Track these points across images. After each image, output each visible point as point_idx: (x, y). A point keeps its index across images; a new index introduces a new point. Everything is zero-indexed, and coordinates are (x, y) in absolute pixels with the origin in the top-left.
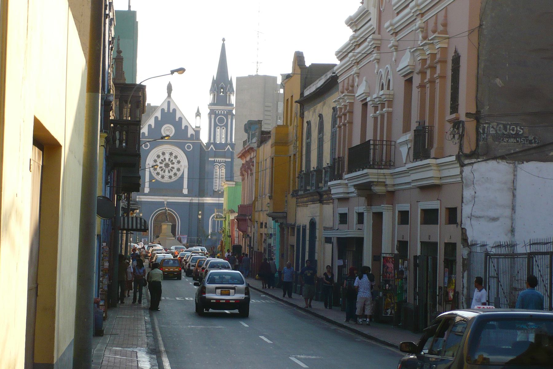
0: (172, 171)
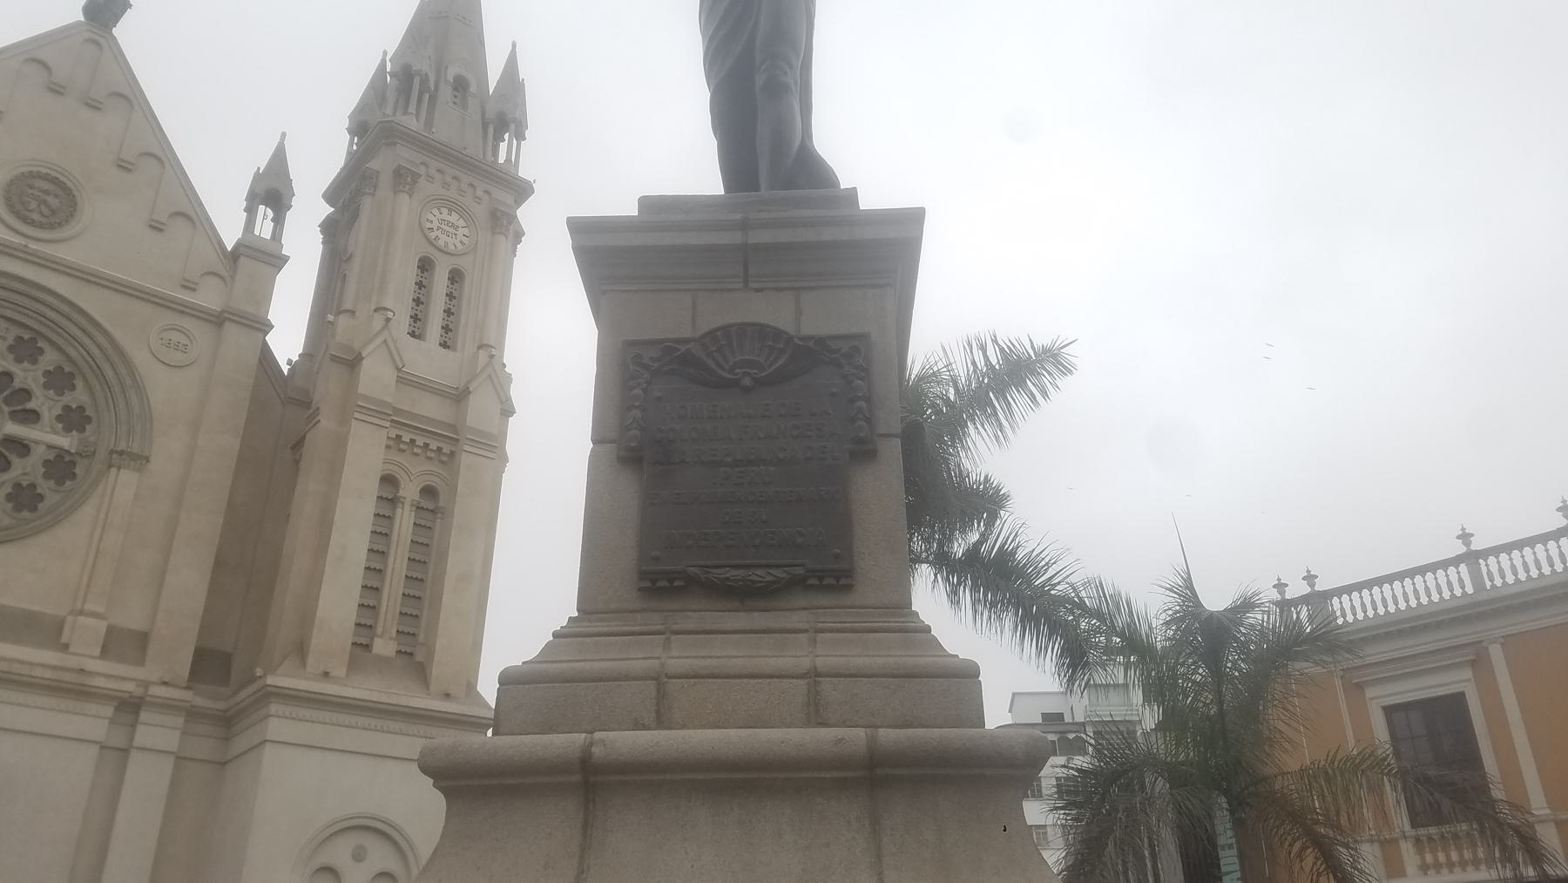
0: (26, 394)
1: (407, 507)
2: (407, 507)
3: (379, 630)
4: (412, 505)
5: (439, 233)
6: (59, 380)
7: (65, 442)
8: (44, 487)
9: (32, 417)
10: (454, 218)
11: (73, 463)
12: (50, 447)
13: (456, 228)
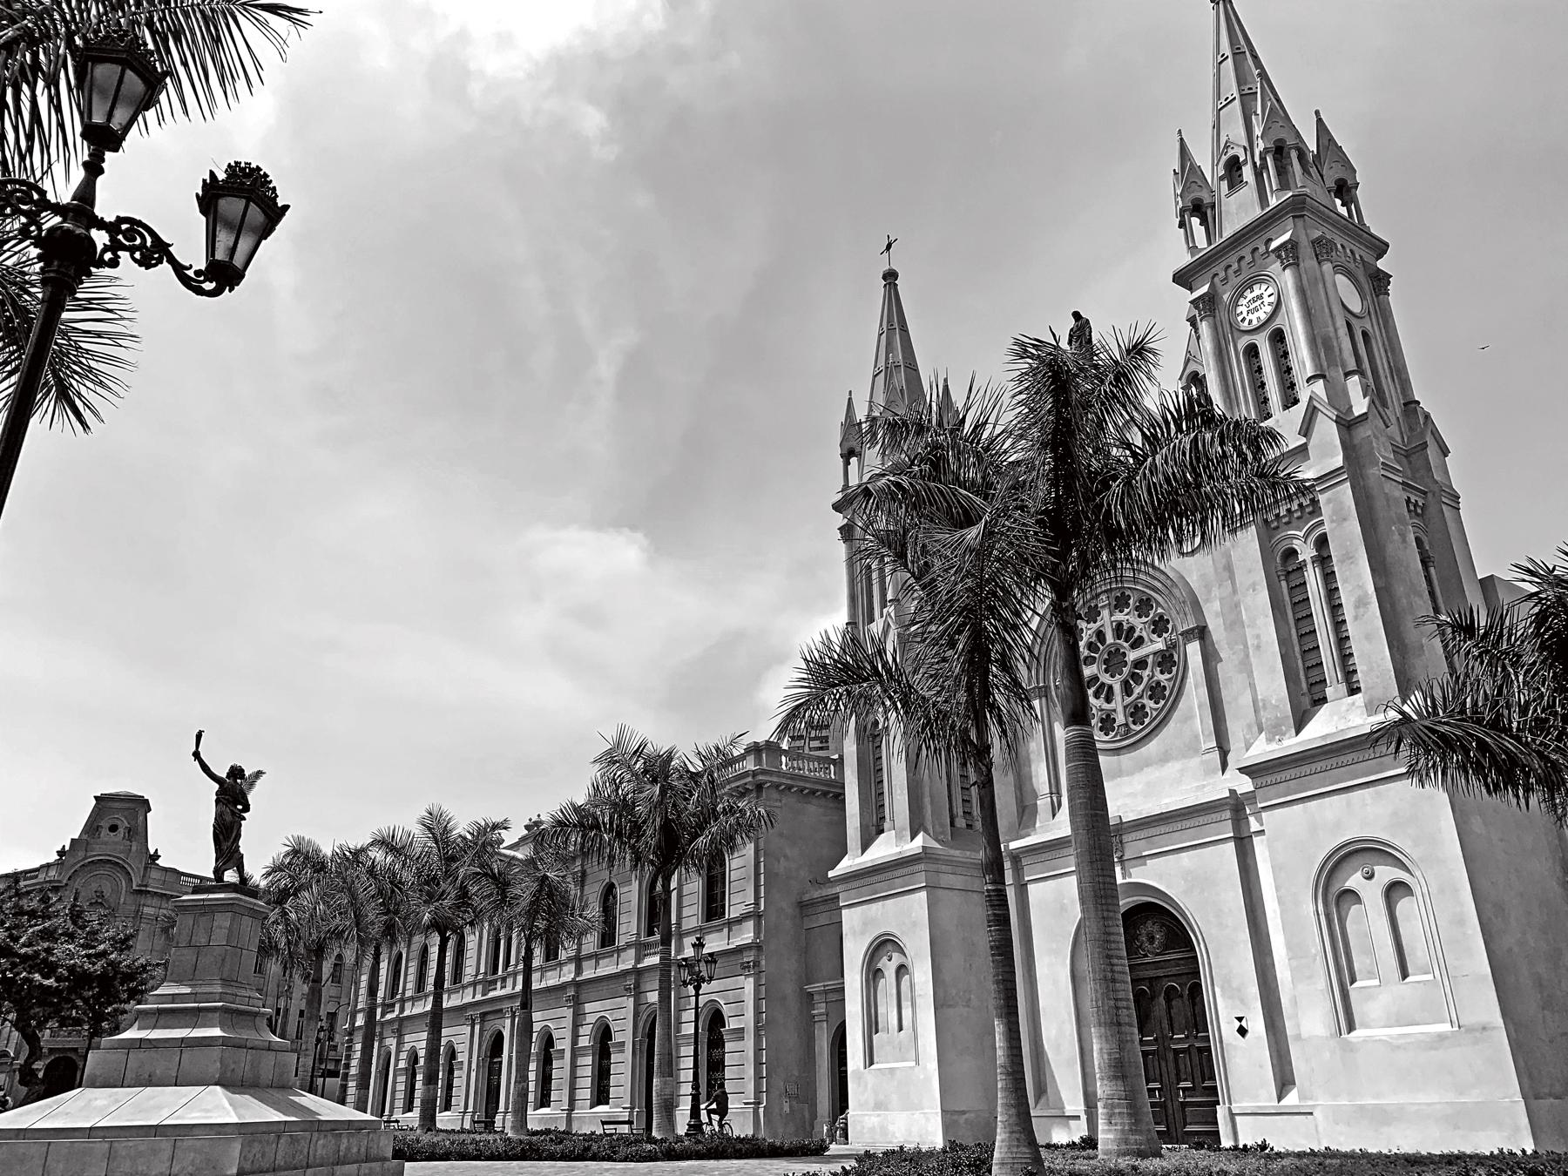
1: (1310, 567)
2: (1310, 567)
3: (1328, 681)
4: (1313, 563)
5: (1251, 316)
6: (1144, 606)
7: (1159, 645)
8: (1163, 678)
9: (1139, 642)
10: (1257, 291)
11: (1172, 655)
12: (1155, 654)
13: (1260, 297)
